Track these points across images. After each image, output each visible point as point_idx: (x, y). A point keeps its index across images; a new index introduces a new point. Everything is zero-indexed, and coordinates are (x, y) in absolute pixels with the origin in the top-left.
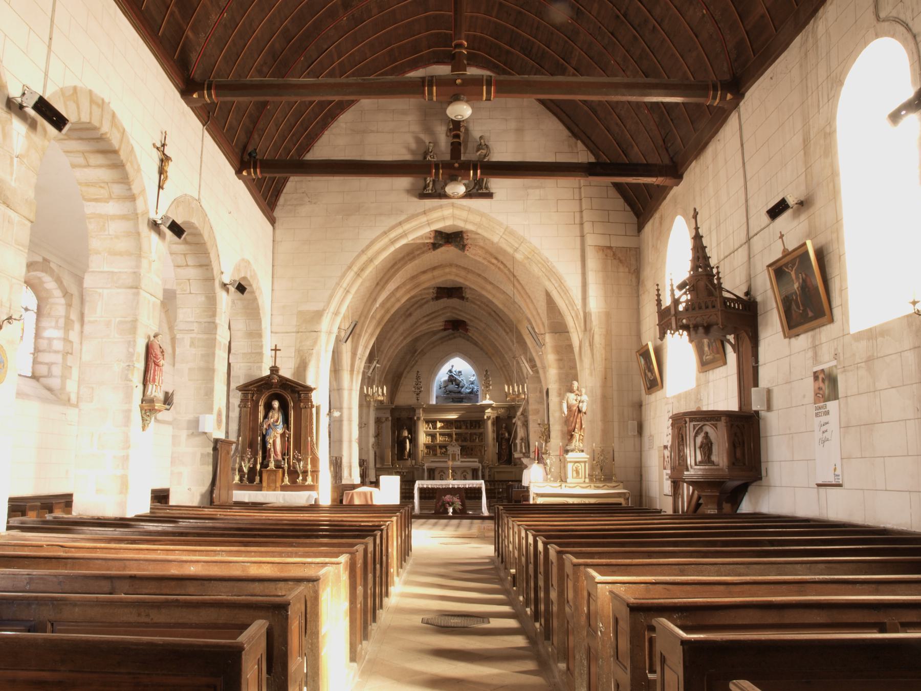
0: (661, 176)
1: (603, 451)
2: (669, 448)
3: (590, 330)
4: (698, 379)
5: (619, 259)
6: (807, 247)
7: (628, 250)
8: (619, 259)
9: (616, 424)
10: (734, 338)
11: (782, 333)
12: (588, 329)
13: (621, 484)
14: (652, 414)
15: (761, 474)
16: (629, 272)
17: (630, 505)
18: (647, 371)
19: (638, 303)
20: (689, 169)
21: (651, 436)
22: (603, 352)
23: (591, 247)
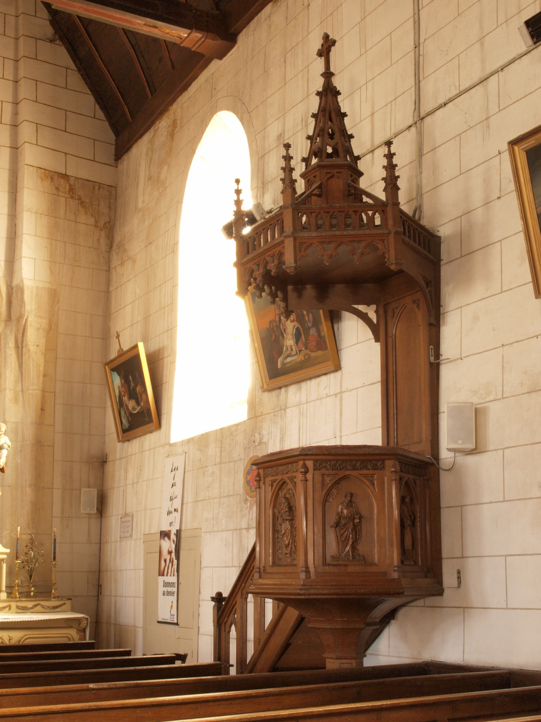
0: (199, 29)
1: (32, 541)
2: (173, 537)
3: (20, 318)
4: (253, 405)
5: (80, 199)
6: (138, 350)
7: (97, 188)
8: (80, 199)
9: (57, 494)
10: (376, 312)
11: (531, 286)
12: (14, 318)
13: (68, 602)
14: (131, 475)
15: (440, 582)
16: (96, 226)
17: (88, 641)
18: (125, 399)
19: (108, 282)
20: (252, 24)
21: (126, 515)
22: (42, 361)
23: (31, 168)
